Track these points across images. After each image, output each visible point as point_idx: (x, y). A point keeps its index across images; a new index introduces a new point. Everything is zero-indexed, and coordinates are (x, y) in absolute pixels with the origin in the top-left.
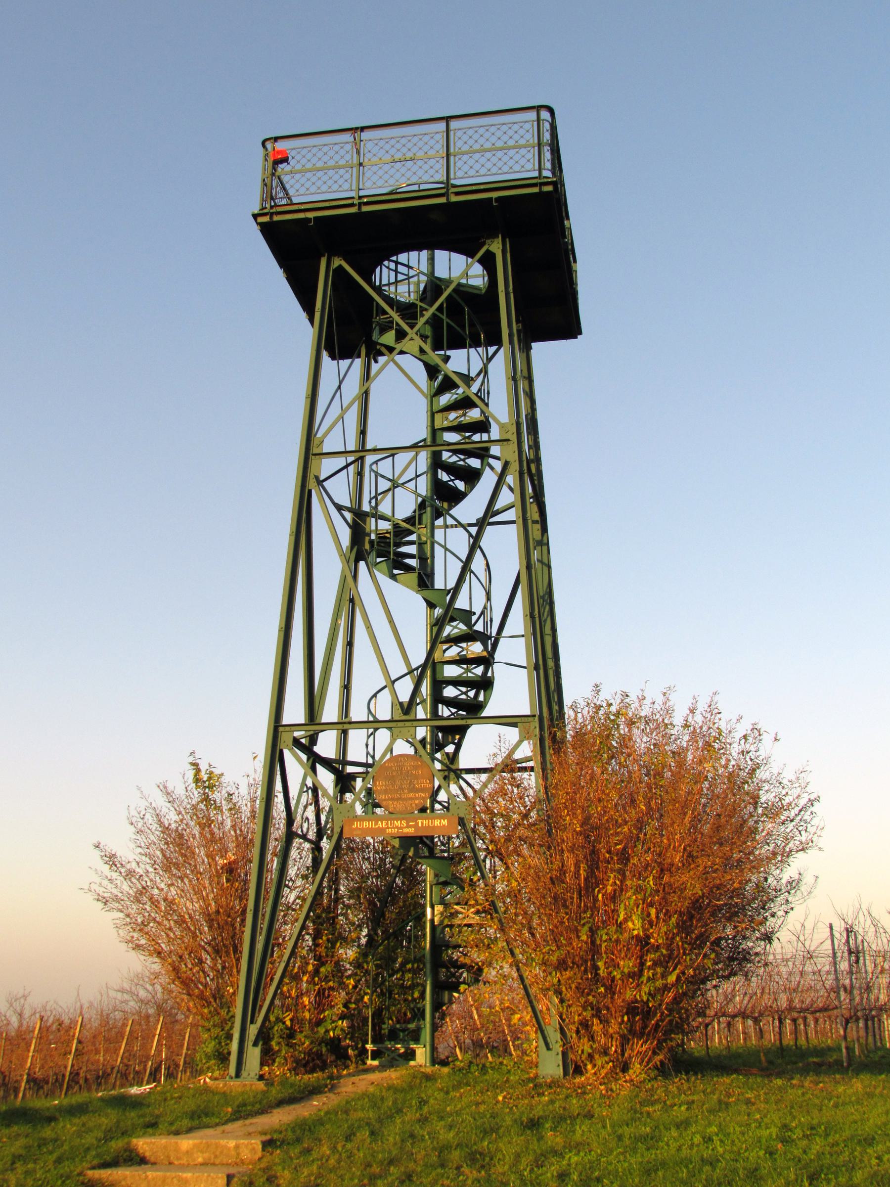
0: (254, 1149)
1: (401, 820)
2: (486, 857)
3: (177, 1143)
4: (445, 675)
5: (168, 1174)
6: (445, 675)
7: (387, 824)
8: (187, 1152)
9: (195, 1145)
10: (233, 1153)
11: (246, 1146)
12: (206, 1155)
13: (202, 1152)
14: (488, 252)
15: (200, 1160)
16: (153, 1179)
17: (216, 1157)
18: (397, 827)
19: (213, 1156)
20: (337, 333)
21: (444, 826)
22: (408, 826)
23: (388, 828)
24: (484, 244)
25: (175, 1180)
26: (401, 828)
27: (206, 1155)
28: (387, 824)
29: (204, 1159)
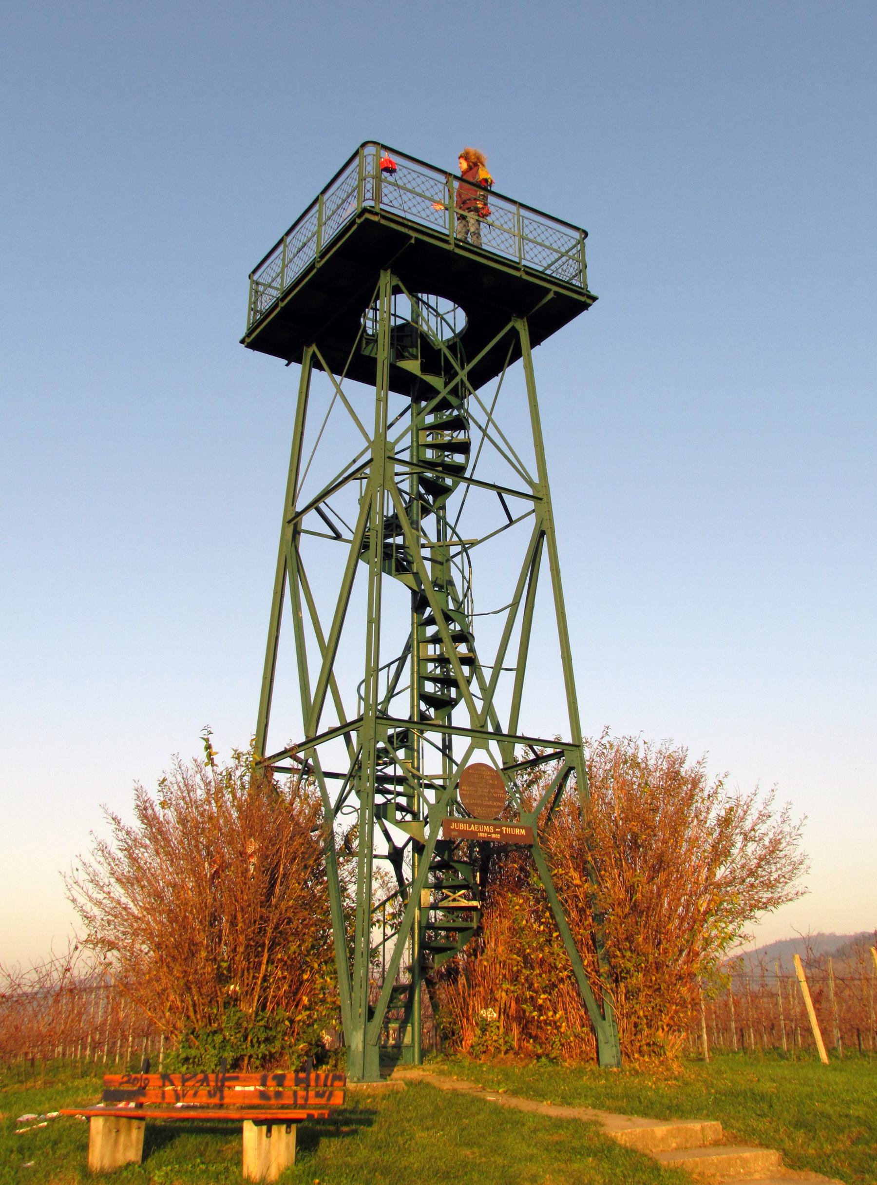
0: (716, 1129)
1: (489, 825)
2: (251, 856)
3: (652, 1131)
4: (426, 690)
5: (731, 1155)
6: (426, 690)
7: (478, 828)
8: (662, 1138)
9: (668, 1131)
10: (700, 1136)
11: (710, 1128)
12: (678, 1140)
13: (674, 1137)
14: (513, 328)
15: (674, 1145)
16: (720, 1162)
17: (687, 1141)
18: (486, 832)
19: (684, 1140)
20: (350, 353)
21: (523, 835)
22: (495, 832)
23: (479, 832)
24: (510, 320)
25: (738, 1161)
26: (490, 833)
27: (678, 1140)
28: (478, 828)
29: (677, 1143)
